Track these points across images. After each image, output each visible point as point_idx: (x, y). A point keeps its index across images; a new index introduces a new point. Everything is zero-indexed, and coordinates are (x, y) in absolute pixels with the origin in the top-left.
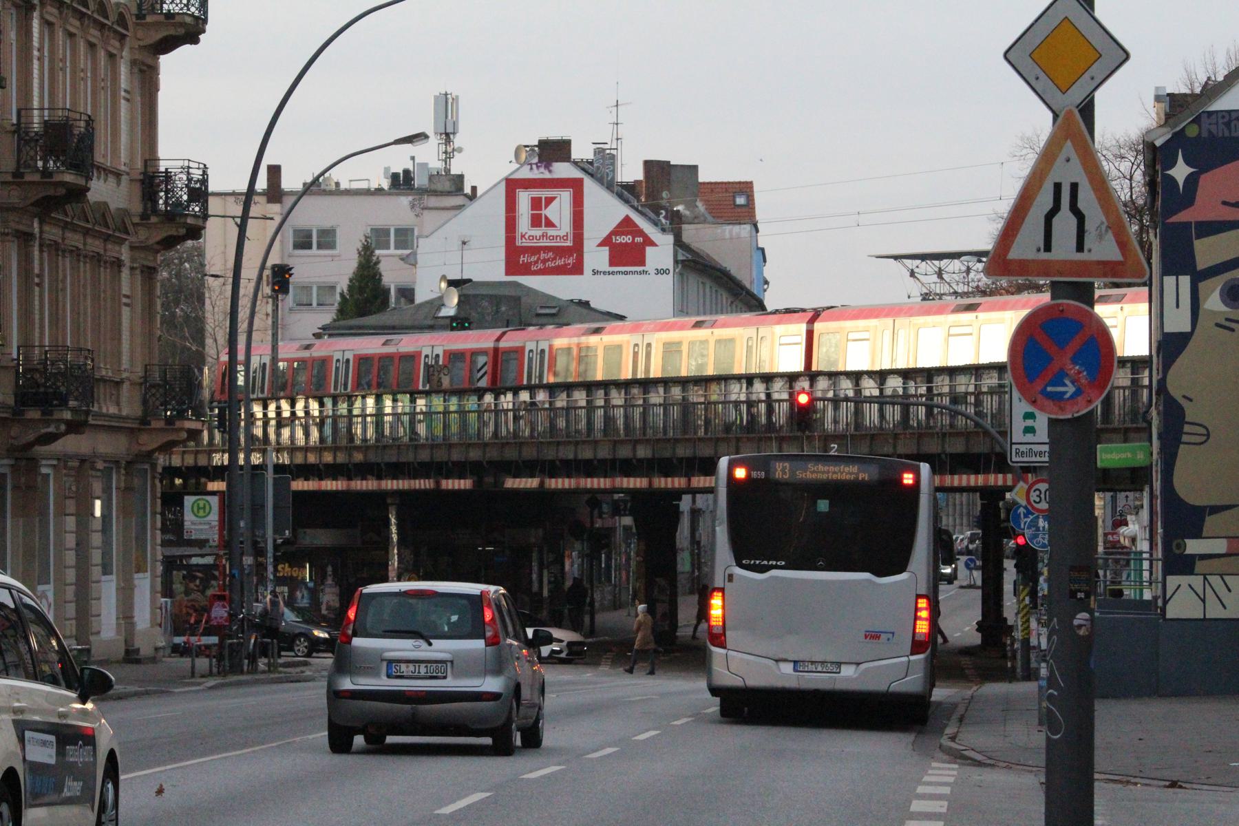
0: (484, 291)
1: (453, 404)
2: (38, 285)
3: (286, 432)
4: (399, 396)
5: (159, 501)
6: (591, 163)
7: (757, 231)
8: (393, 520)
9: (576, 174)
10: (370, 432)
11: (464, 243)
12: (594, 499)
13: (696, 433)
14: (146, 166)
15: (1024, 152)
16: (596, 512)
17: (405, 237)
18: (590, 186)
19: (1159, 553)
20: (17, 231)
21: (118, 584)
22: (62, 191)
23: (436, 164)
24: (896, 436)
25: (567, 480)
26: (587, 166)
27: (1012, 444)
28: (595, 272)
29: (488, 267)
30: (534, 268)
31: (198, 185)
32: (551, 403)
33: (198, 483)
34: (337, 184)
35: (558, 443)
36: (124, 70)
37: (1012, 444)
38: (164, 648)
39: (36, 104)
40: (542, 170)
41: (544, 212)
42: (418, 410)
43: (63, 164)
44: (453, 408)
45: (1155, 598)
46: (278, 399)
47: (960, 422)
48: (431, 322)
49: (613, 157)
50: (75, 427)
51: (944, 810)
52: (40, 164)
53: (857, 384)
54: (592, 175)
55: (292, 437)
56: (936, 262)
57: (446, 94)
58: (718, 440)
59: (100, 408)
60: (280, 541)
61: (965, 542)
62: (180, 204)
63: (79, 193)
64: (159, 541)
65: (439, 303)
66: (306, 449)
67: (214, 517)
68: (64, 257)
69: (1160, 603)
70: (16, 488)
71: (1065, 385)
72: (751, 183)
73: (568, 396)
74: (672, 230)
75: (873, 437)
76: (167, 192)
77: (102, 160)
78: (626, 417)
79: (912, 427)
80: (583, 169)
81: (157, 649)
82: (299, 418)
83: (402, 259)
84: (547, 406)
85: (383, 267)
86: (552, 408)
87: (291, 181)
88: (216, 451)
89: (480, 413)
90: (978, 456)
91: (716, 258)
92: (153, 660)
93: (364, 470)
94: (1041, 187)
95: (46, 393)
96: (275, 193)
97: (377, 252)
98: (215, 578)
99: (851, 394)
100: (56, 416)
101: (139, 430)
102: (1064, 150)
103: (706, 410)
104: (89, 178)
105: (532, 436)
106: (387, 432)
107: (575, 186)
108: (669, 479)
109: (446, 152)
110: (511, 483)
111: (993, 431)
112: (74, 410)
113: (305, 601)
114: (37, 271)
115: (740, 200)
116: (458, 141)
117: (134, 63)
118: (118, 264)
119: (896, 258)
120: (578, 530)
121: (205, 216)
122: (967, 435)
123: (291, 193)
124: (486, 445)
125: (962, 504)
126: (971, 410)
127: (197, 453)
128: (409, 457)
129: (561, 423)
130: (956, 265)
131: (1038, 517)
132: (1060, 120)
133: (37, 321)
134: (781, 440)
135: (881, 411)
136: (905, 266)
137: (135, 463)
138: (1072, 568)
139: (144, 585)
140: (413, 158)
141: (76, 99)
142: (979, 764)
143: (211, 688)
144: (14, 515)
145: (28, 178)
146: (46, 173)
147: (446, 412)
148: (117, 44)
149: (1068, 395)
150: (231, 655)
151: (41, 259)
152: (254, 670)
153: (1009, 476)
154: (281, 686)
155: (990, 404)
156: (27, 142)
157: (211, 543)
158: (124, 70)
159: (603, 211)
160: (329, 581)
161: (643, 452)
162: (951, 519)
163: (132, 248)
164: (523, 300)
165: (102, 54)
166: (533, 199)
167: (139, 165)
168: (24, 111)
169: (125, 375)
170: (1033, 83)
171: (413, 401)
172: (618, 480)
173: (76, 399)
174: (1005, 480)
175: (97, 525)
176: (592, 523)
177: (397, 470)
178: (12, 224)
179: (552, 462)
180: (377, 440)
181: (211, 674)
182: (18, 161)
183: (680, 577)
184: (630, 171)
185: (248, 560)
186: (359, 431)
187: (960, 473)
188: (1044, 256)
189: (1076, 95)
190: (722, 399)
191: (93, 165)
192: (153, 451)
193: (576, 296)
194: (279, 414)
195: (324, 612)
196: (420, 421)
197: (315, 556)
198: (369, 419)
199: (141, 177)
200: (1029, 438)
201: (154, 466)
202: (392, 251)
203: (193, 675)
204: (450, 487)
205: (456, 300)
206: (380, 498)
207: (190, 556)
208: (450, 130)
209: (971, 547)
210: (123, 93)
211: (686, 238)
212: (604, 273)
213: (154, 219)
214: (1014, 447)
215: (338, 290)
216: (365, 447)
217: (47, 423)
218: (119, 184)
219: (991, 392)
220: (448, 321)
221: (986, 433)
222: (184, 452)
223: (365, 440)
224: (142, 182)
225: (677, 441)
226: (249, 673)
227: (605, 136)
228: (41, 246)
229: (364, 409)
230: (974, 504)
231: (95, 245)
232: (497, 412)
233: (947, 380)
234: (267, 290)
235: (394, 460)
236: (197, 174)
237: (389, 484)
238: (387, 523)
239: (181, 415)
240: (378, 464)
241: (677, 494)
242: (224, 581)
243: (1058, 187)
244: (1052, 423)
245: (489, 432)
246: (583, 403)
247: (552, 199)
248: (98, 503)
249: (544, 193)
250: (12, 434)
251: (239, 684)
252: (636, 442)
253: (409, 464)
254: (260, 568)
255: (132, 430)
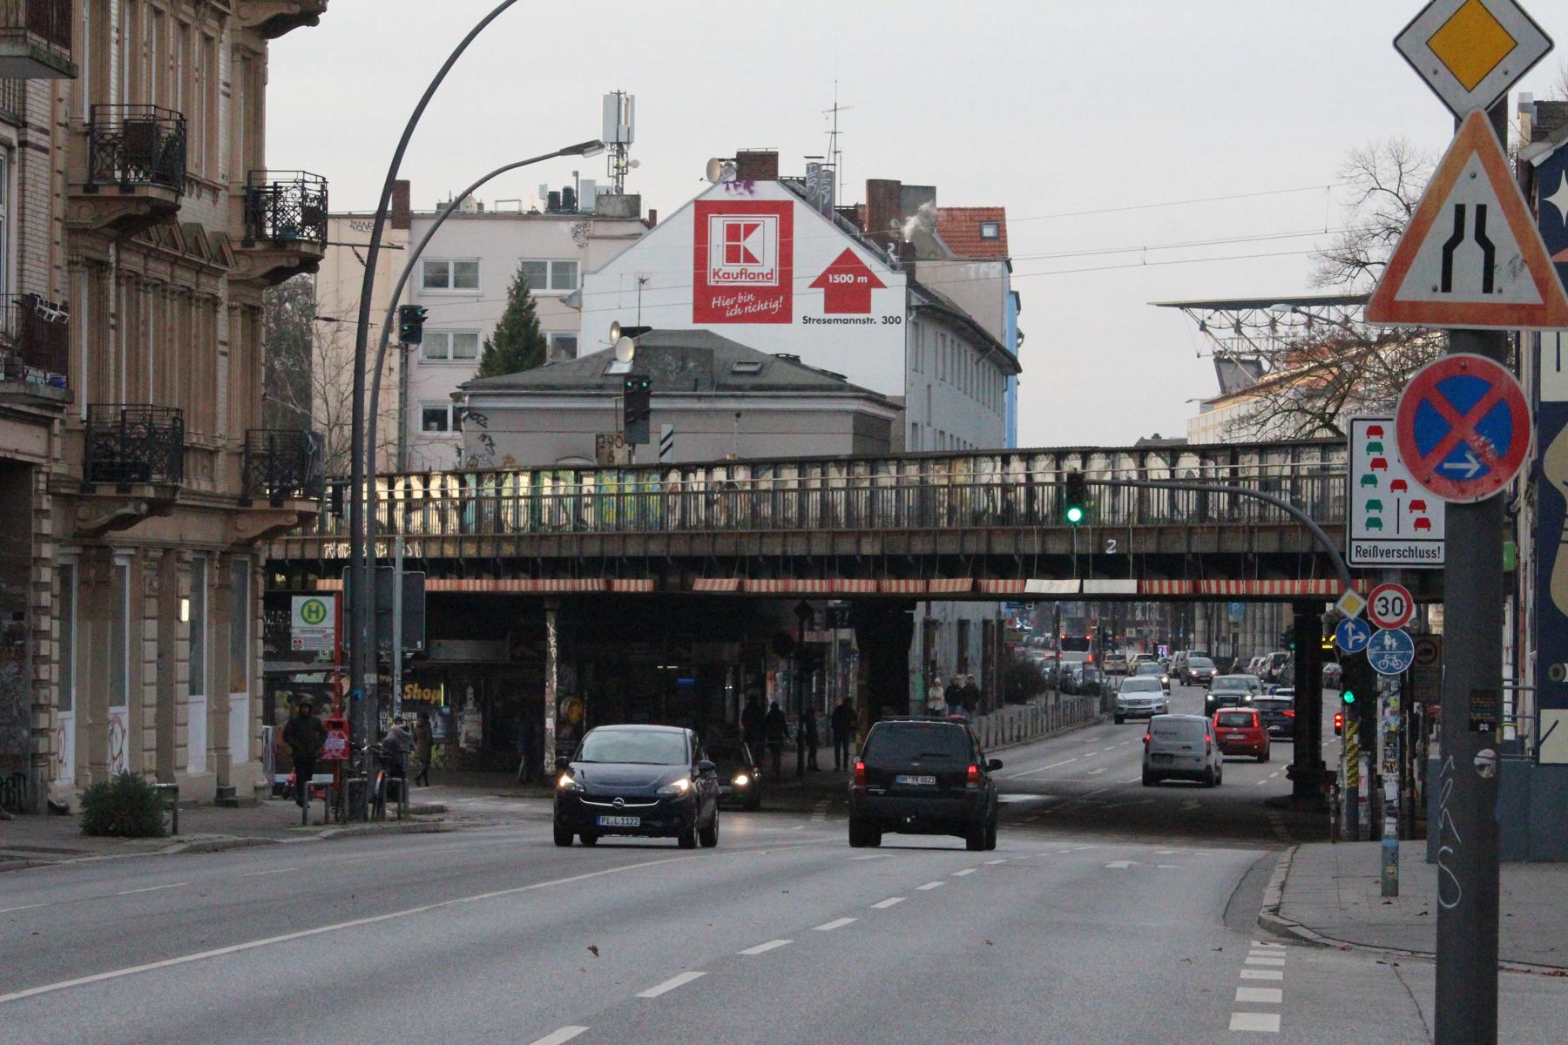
0: (667, 343)
1: (630, 483)
2: (113, 327)
3: (417, 518)
4: (561, 474)
5: (261, 603)
6: (803, 182)
7: (1010, 270)
8: (552, 630)
9: (784, 195)
10: (524, 519)
11: (642, 281)
12: (804, 605)
13: (936, 524)
14: (249, 180)
15: (1356, 172)
16: (806, 624)
17: (565, 273)
18: (801, 211)
19: (1529, 679)
20: (88, 259)
21: (209, 706)
22: (144, 209)
23: (605, 182)
24: (1190, 531)
25: (772, 582)
26: (798, 186)
27: (1351, 540)
28: (807, 320)
29: (672, 312)
30: (729, 314)
31: (315, 204)
32: (753, 484)
33: (305, 581)
34: (480, 205)
35: (762, 535)
36: (223, 56)
37: (1351, 540)
38: (263, 788)
39: (113, 99)
40: (741, 189)
41: (742, 243)
42: (585, 491)
43: (146, 174)
44: (628, 490)
45: (1521, 739)
46: (408, 475)
47: (1273, 512)
48: (599, 381)
49: (831, 175)
50: (159, 508)
51: (1279, 1000)
52: (118, 174)
53: (1142, 464)
54: (804, 197)
55: (425, 524)
56: (1234, 313)
57: (619, 94)
58: (964, 532)
59: (189, 483)
60: (409, 655)
61: (1268, 667)
62: (293, 228)
63: (166, 212)
64: (261, 653)
65: (609, 357)
66: (443, 539)
67: (329, 623)
68: (146, 292)
69: (1529, 743)
70: (84, 583)
71: (1467, 461)
72: (1003, 209)
73: (775, 475)
74: (903, 268)
75: (1161, 531)
76: (275, 212)
77: (195, 171)
78: (848, 503)
79: (1211, 519)
80: (793, 190)
81: (256, 789)
82: (434, 500)
83: (563, 301)
84: (748, 487)
85: (539, 311)
86: (755, 490)
87: (422, 201)
88: (329, 541)
89: (663, 496)
90: (1293, 556)
91: (961, 306)
92: (253, 803)
93: (515, 567)
94: (1438, 209)
95: (123, 465)
96: (404, 218)
97: (533, 292)
98: (329, 700)
99: (1134, 476)
100: (136, 493)
101: (237, 512)
102: (1469, 162)
103: (950, 494)
104: (179, 193)
105: (728, 525)
106: (545, 518)
107: (783, 210)
108: (903, 582)
109: (617, 167)
110: (702, 585)
111: (1315, 525)
112: (157, 486)
113: (439, 731)
114: (112, 310)
115: (989, 231)
116: (633, 153)
117: (235, 48)
118: (214, 302)
119: (1182, 306)
120: (785, 645)
121: (324, 244)
122: (1280, 530)
123: (423, 217)
124: (670, 536)
125: (1263, 618)
126: (1286, 499)
127: (304, 542)
128: (572, 551)
129: (766, 510)
130: (1260, 316)
131: (1383, 633)
132: (1463, 125)
133: (112, 373)
134: (1045, 533)
135: (1172, 498)
136: (1194, 316)
137: (231, 554)
138: (1474, 692)
139: (242, 708)
140: (576, 174)
141: (164, 94)
142: (1310, 943)
143: (327, 838)
144: (79, 619)
145: (106, 192)
146: (125, 186)
147: (620, 495)
148: (215, 24)
149: (1470, 475)
150: (351, 795)
151: (118, 297)
152: (380, 816)
153: (1334, 583)
154: (414, 837)
155: (1310, 491)
156: (102, 148)
157: (321, 656)
158: (223, 56)
159: (817, 244)
160: (470, 706)
161: (869, 548)
162: (1249, 636)
163: (231, 282)
164: (716, 355)
165: (196, 38)
166: (729, 226)
167: (241, 177)
168: (98, 107)
169: (220, 443)
170: (1430, 77)
171: (578, 479)
172: (837, 582)
173: (161, 472)
174: (1328, 587)
175: (184, 632)
176: (802, 636)
177: (556, 567)
178: (84, 252)
179: (754, 559)
180: (533, 529)
181: (327, 821)
182: (91, 170)
183: (912, 705)
184: (852, 194)
185: (371, 679)
186: (509, 518)
187: (1272, 578)
188: (1442, 297)
189: (1484, 94)
190: (970, 481)
191: (184, 177)
192: (255, 539)
193: (783, 350)
194: (408, 494)
195: (463, 745)
196: (587, 506)
197: (447, 674)
198: (522, 502)
199: (244, 193)
200: (1374, 532)
201: (255, 557)
202: (549, 291)
203: (305, 822)
204: (625, 589)
205: (631, 354)
206: (534, 604)
207: (295, 673)
208: (622, 139)
209: (1275, 672)
210: (222, 87)
211: (921, 277)
212: (818, 321)
213: (259, 246)
214: (1354, 544)
215: (481, 340)
216: (517, 538)
217: (124, 502)
218: (215, 202)
219: (1312, 476)
220: (621, 380)
221: (1305, 527)
222: (288, 541)
223: (517, 529)
224: (245, 198)
225: (912, 533)
226: (374, 820)
227: (820, 148)
228: (118, 278)
229: (516, 489)
230: (1280, 619)
231: (185, 278)
232: (685, 494)
233: (1256, 460)
234: (394, 338)
235: (554, 554)
236: (313, 190)
237: (548, 585)
238: (544, 634)
239: (286, 493)
240: (534, 560)
241: (910, 601)
242: (341, 702)
243: (1460, 210)
244: (1450, 508)
245: (674, 519)
246: (794, 485)
247: (755, 226)
248: (185, 604)
249: (743, 220)
250: (81, 515)
251: (363, 834)
252: (859, 536)
253: (573, 559)
254: (384, 689)
255: (228, 512)
